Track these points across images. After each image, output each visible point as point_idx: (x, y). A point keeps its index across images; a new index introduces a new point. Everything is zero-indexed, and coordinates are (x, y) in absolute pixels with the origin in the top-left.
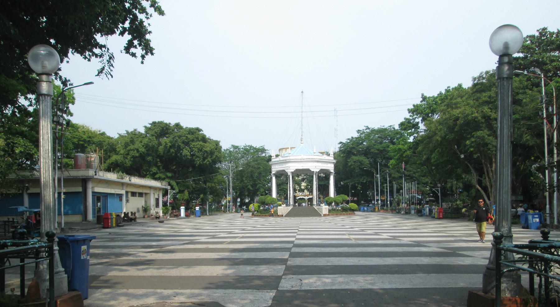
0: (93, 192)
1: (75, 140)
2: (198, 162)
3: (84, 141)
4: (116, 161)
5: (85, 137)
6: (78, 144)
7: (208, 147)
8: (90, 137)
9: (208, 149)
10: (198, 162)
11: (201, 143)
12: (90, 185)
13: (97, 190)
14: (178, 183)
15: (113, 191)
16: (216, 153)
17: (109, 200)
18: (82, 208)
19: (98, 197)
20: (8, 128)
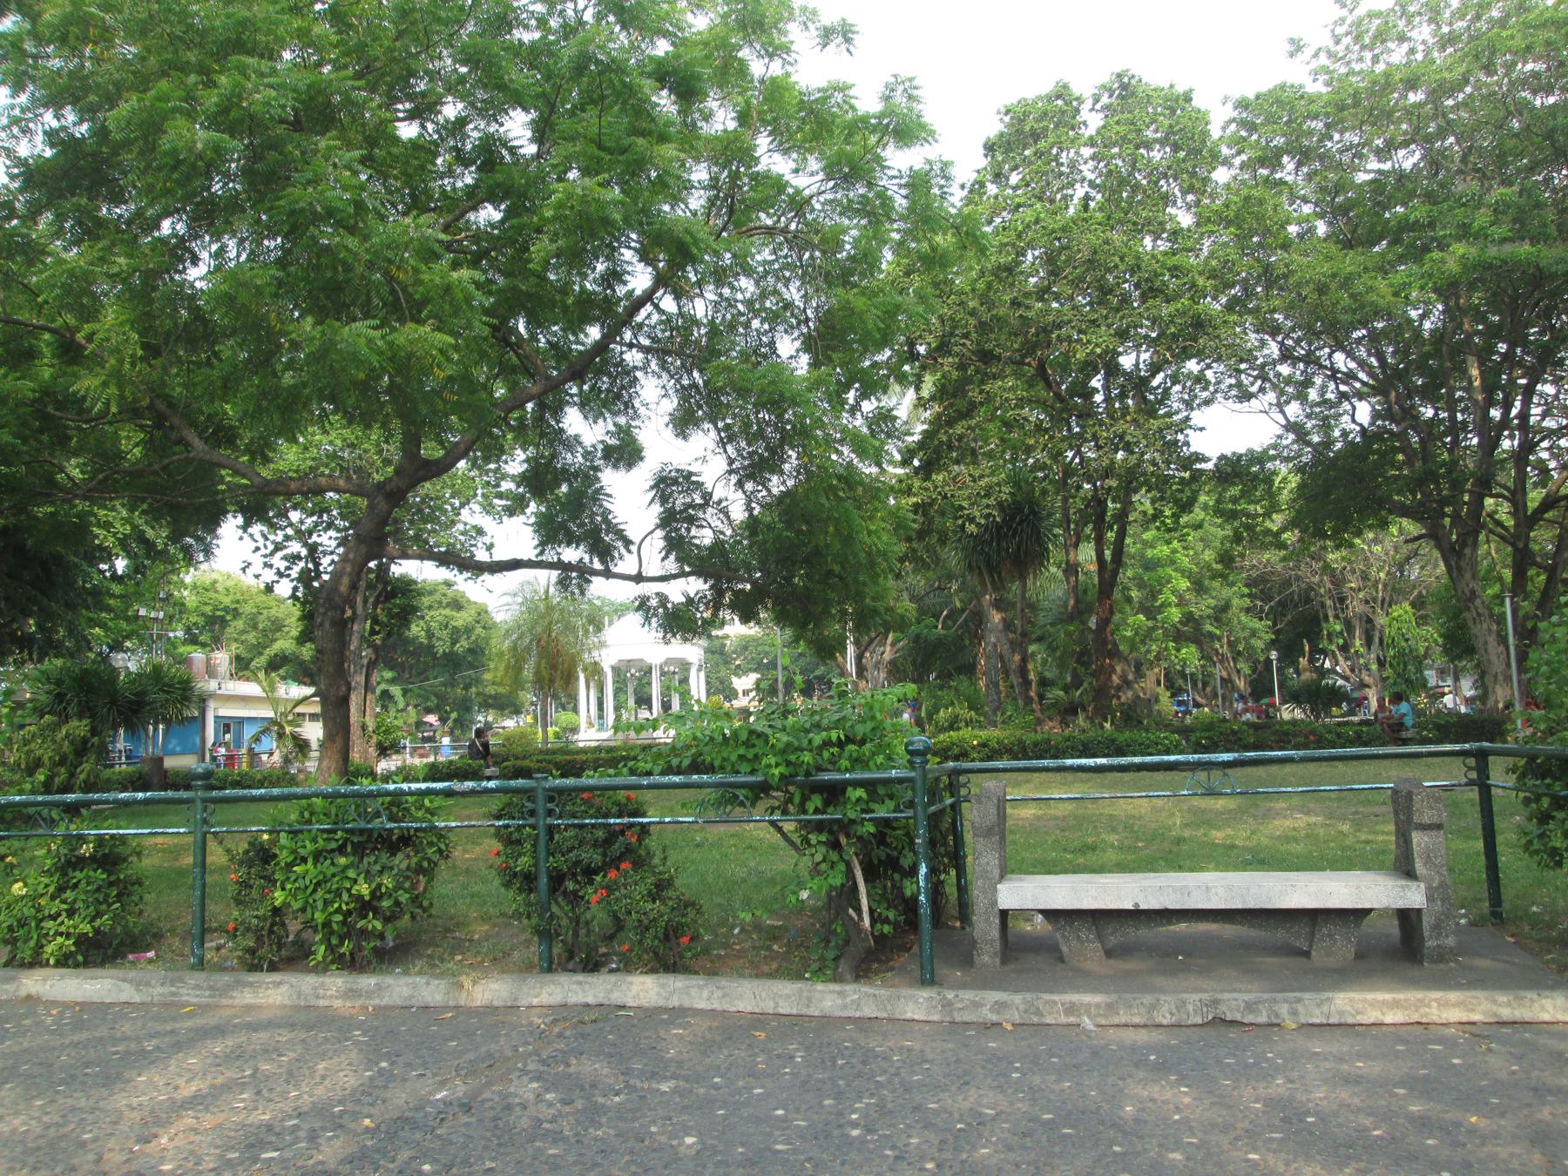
0: (216, 717)
1: (207, 609)
2: (441, 648)
3: (226, 609)
4: (283, 651)
5: (227, 601)
6: (213, 616)
7: (461, 619)
8: (238, 602)
9: (459, 623)
10: (441, 648)
11: (448, 612)
12: (212, 705)
13: (223, 712)
14: (405, 692)
15: (253, 714)
16: (479, 630)
17: (1491, 758)
18: (198, 741)
19: (225, 725)
20: (61, 643)
